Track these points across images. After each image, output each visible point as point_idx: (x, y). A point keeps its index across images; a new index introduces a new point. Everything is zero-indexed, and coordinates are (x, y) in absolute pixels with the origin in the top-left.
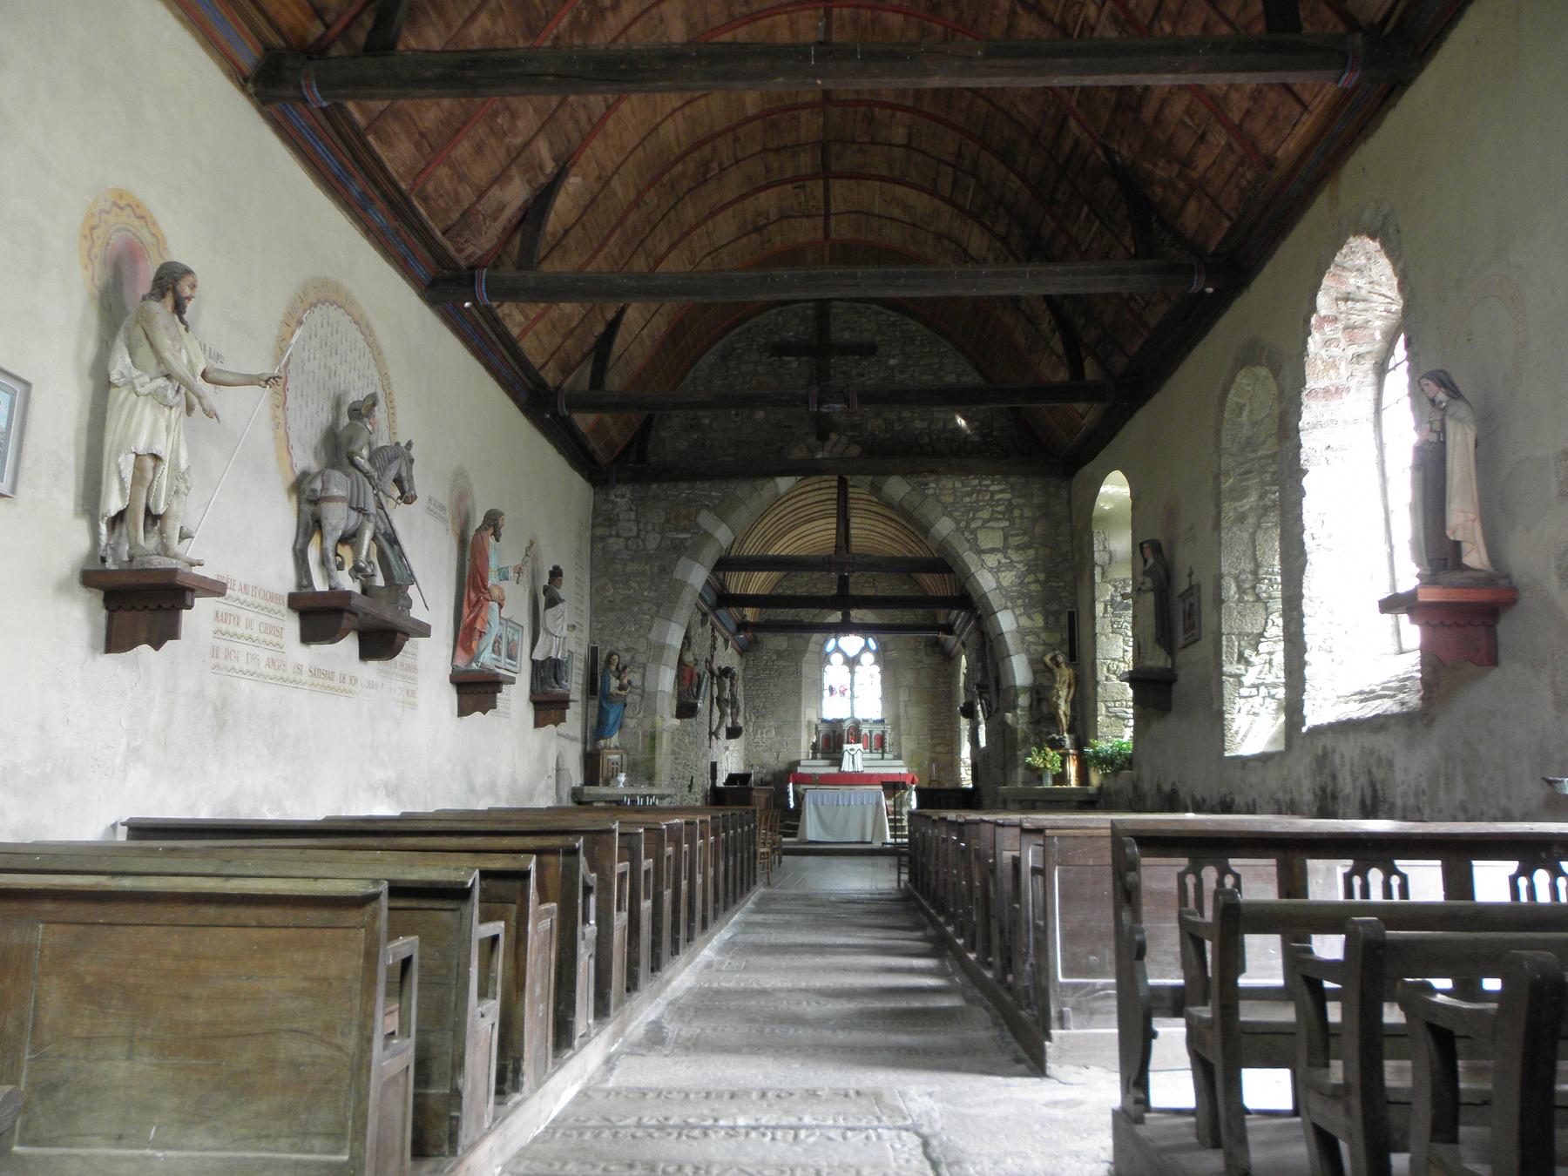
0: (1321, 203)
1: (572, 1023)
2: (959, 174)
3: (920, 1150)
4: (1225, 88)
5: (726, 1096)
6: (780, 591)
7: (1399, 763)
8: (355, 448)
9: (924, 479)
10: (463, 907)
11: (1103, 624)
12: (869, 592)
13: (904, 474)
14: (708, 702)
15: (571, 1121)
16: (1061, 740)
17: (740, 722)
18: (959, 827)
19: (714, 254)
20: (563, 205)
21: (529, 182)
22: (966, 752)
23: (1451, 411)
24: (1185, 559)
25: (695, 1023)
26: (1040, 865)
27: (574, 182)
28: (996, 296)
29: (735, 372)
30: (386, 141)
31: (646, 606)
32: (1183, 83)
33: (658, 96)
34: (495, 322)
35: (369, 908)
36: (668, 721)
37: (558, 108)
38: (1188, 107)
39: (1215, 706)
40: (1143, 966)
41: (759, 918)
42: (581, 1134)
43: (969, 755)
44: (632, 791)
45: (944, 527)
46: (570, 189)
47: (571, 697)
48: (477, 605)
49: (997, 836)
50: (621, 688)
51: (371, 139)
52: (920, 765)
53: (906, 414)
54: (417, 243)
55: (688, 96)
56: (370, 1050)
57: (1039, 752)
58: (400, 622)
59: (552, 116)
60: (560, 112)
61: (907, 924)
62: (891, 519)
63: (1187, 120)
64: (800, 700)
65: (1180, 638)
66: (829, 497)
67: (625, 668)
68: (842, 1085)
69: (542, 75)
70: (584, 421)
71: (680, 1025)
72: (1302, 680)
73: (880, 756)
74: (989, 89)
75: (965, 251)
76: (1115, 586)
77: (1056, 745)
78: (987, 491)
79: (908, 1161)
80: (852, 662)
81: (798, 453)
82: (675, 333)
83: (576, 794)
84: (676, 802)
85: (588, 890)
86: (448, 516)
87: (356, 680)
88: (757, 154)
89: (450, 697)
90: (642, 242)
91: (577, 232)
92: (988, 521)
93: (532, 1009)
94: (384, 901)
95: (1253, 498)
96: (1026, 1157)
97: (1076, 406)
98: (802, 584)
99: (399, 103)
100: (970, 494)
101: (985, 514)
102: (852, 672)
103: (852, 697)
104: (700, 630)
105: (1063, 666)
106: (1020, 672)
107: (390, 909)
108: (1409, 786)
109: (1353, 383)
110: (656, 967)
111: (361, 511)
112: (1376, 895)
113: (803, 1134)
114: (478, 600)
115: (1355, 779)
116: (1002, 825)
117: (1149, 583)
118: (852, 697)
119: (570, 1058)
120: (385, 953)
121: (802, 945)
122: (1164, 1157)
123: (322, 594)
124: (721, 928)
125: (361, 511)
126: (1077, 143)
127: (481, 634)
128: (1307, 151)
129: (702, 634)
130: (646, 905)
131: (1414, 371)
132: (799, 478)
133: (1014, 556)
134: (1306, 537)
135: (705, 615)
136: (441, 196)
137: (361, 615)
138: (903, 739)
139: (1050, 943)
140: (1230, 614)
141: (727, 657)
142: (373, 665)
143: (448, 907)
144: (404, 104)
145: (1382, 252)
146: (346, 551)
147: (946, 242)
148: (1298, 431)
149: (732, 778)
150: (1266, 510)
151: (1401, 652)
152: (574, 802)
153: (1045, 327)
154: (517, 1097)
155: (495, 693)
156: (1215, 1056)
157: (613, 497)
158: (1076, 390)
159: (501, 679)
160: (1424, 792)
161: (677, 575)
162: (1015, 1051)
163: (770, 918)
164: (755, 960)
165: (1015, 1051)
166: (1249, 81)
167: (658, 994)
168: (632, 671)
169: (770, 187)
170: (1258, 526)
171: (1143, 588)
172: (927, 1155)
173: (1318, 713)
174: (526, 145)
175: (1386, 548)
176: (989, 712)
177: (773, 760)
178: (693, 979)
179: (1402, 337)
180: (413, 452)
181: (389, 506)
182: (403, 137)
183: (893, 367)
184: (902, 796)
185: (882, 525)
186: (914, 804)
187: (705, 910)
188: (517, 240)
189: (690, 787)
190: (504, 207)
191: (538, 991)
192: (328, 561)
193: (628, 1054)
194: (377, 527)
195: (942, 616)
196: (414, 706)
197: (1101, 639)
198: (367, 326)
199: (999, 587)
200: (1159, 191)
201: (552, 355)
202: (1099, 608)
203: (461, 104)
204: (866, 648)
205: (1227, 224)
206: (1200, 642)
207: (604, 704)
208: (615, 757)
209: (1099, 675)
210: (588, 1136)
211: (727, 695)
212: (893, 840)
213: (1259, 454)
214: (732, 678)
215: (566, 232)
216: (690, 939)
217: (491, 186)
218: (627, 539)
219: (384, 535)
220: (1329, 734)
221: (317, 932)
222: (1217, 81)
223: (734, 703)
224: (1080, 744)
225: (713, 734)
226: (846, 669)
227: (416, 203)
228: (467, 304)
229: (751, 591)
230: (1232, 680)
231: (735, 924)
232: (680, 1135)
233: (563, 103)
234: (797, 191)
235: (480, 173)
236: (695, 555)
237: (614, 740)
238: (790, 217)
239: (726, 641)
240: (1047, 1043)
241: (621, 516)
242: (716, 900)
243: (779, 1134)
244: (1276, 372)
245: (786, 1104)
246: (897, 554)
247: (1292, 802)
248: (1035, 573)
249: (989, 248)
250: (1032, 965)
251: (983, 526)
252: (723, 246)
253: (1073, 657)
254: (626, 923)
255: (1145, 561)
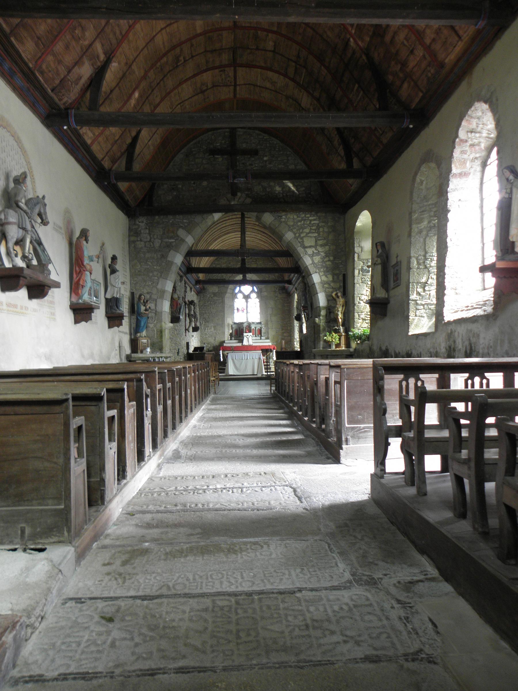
0: (464, 85)
1: (144, 451)
2: (298, 66)
3: (293, 493)
4: (424, 27)
5: (211, 477)
6: (214, 266)
7: (482, 336)
8: (19, 199)
9: (280, 215)
10: (100, 404)
11: (358, 279)
12: (254, 266)
13: (271, 212)
14: (184, 316)
15: (147, 490)
16: (339, 329)
17: (198, 324)
18: (300, 366)
19: (182, 104)
20: (110, 77)
21: (93, 65)
22: (297, 336)
23: (515, 184)
24: (395, 250)
25: (193, 449)
26: (339, 380)
27: (114, 65)
28: (314, 128)
29: (193, 163)
30: (21, 42)
31: (155, 273)
32: (407, 24)
33: (154, 22)
34: (79, 137)
35: (64, 405)
36: (168, 325)
37: (105, 26)
38: (407, 35)
39: (406, 313)
40: (385, 418)
41: (213, 407)
42: (152, 495)
43: (298, 337)
44: (153, 355)
45: (289, 236)
46: (113, 69)
47: (125, 315)
48: (80, 273)
49: (318, 370)
50: (146, 310)
51: (12, 39)
52: (277, 342)
53: (272, 184)
54: (39, 95)
55: (168, 22)
56: (70, 463)
57: (330, 335)
58: (47, 282)
59: (103, 30)
60: (106, 28)
61: (276, 407)
62: (264, 233)
63: (405, 42)
64: (224, 314)
65: (392, 284)
66: (236, 222)
67: (147, 301)
68: (258, 470)
69: (100, 8)
70: (123, 186)
71: (187, 451)
72: (443, 302)
73: (259, 338)
74: (313, 24)
75: (300, 105)
76: (363, 263)
77: (337, 331)
78: (308, 219)
79: (288, 498)
80: (247, 297)
81: (223, 202)
82: (164, 143)
83: (128, 357)
84: (172, 359)
85: (147, 396)
86: (63, 232)
87: (28, 308)
88: (202, 53)
89: (70, 316)
90: (147, 98)
91: (116, 91)
92: (309, 233)
93: (128, 445)
94: (70, 401)
95: (425, 223)
96: (336, 494)
97: (348, 180)
98: (224, 262)
99: (26, 20)
100: (300, 221)
101: (307, 230)
102: (247, 302)
103: (247, 312)
104: (179, 284)
105: (340, 297)
106: (322, 300)
107: (73, 406)
108: (485, 344)
109: (472, 170)
110: (174, 428)
111: (24, 229)
112: (477, 387)
113: (244, 490)
114: (80, 271)
115: (463, 343)
116: (321, 365)
117: (379, 261)
118: (247, 312)
119: (144, 465)
120: (73, 424)
121: (233, 417)
122: (393, 490)
123: (9, 268)
124: (198, 411)
125: (24, 229)
126: (354, 53)
127: (83, 286)
128: (459, 60)
129: (180, 286)
130: (169, 402)
131: (500, 165)
132: (223, 214)
133: (320, 249)
134: (448, 240)
135: (181, 277)
136: (50, 71)
137: (28, 278)
138: (270, 331)
139: (342, 411)
140: (414, 274)
141: (191, 296)
142: (35, 301)
143: (93, 404)
144: (29, 21)
145: (489, 110)
146: (18, 248)
147: (291, 100)
148: (447, 192)
149: (196, 349)
150: (431, 228)
151: (484, 289)
152: (127, 360)
153: (336, 143)
154: (125, 481)
155: (90, 313)
156: (414, 450)
157: (138, 223)
158: (349, 173)
159: (93, 307)
160: (491, 347)
161: (169, 259)
162: (326, 455)
163: (218, 407)
164: (214, 424)
165: (326, 455)
166: (435, 23)
167: (175, 439)
168: (150, 303)
169: (208, 71)
170: (427, 235)
171: (377, 263)
172: (295, 495)
173: (449, 316)
174: (90, 45)
175: (481, 245)
176: (308, 318)
177: (213, 341)
178: (189, 432)
179: (495, 149)
180: (46, 201)
181: (37, 226)
182: (29, 39)
183: (266, 161)
184: (270, 354)
185: (260, 236)
186: (275, 358)
187: (191, 404)
188: (88, 95)
189: (178, 353)
190: (81, 78)
191: (130, 438)
192: (11, 253)
193: (166, 463)
194: (32, 237)
195: (286, 277)
196: (54, 319)
197: (357, 286)
198: (18, 138)
199: (313, 263)
200: (390, 77)
201: (107, 153)
202: (356, 272)
203: (57, 22)
204: (253, 291)
205: (421, 94)
206: (401, 286)
207: (139, 318)
208: (145, 341)
209: (356, 301)
210: (155, 495)
211: (192, 313)
212: (266, 374)
213: (429, 203)
214: (194, 305)
215: (112, 91)
216: (186, 416)
217: (73, 67)
218: (145, 242)
219: (36, 240)
220: (454, 324)
221: (41, 416)
222: (420, 23)
223: (195, 316)
224: (347, 331)
225: (187, 330)
226: (244, 300)
227: (38, 75)
228: (65, 128)
229: (202, 266)
230: (413, 302)
231: (203, 409)
232: (194, 493)
233: (107, 23)
234: (221, 73)
235: (68, 59)
236: (176, 249)
237: (144, 333)
238: (217, 86)
239: (191, 289)
240: (341, 451)
241: (142, 232)
242: (195, 400)
243: (235, 490)
244: (439, 165)
245: (236, 479)
246: (266, 249)
247: (437, 352)
248: (329, 257)
249: (311, 104)
250: (333, 421)
251: (306, 236)
252: (186, 100)
253: (344, 294)
254: (162, 410)
255: (378, 251)
